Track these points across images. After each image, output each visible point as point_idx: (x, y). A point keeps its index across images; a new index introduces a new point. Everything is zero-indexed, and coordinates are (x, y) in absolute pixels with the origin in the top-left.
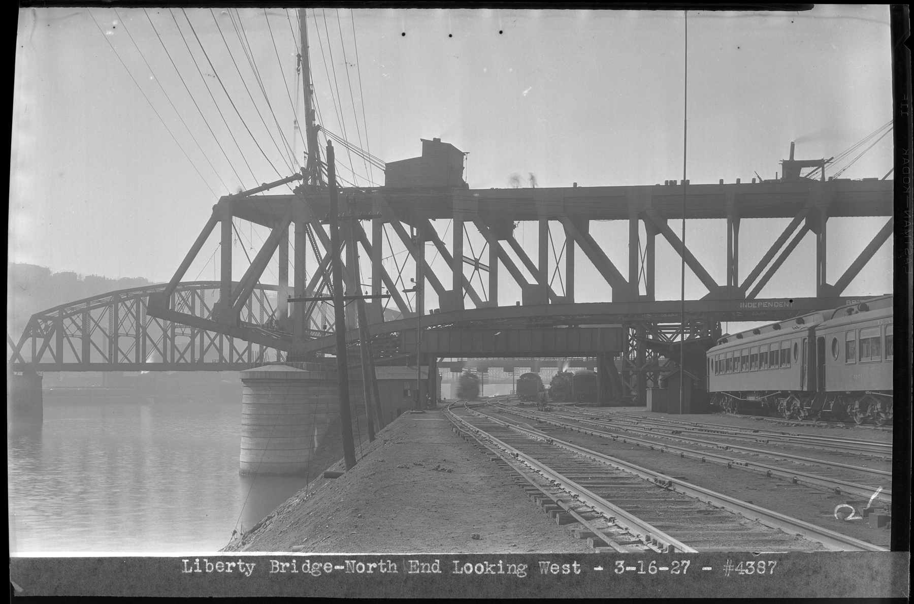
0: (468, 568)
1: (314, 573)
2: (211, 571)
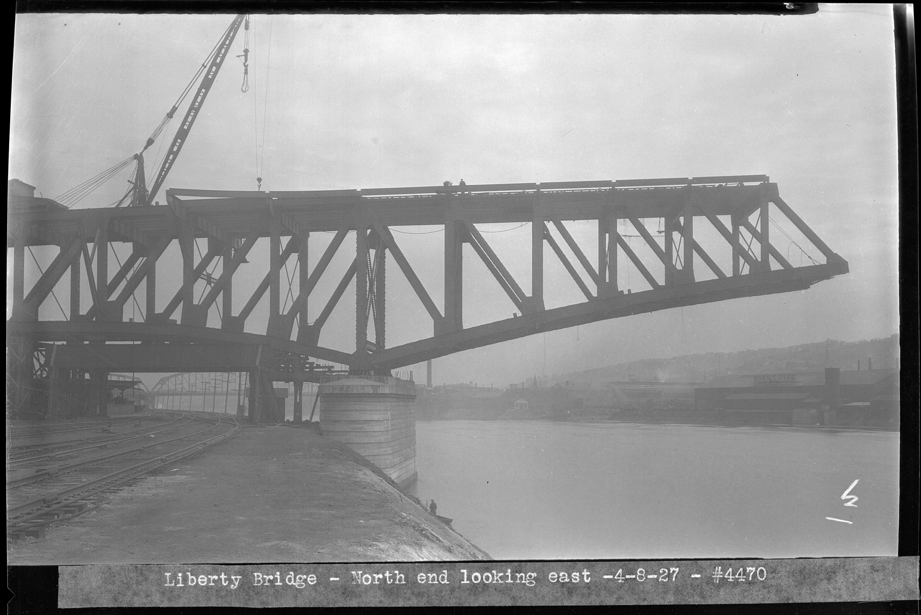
1: (299, 585)
2: (193, 584)
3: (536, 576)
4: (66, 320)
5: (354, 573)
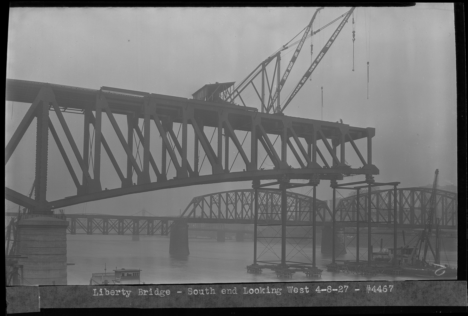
0: (251, 291)
1: (161, 295)
3: (281, 290)
4: (355, 141)
5: (288, 287)
